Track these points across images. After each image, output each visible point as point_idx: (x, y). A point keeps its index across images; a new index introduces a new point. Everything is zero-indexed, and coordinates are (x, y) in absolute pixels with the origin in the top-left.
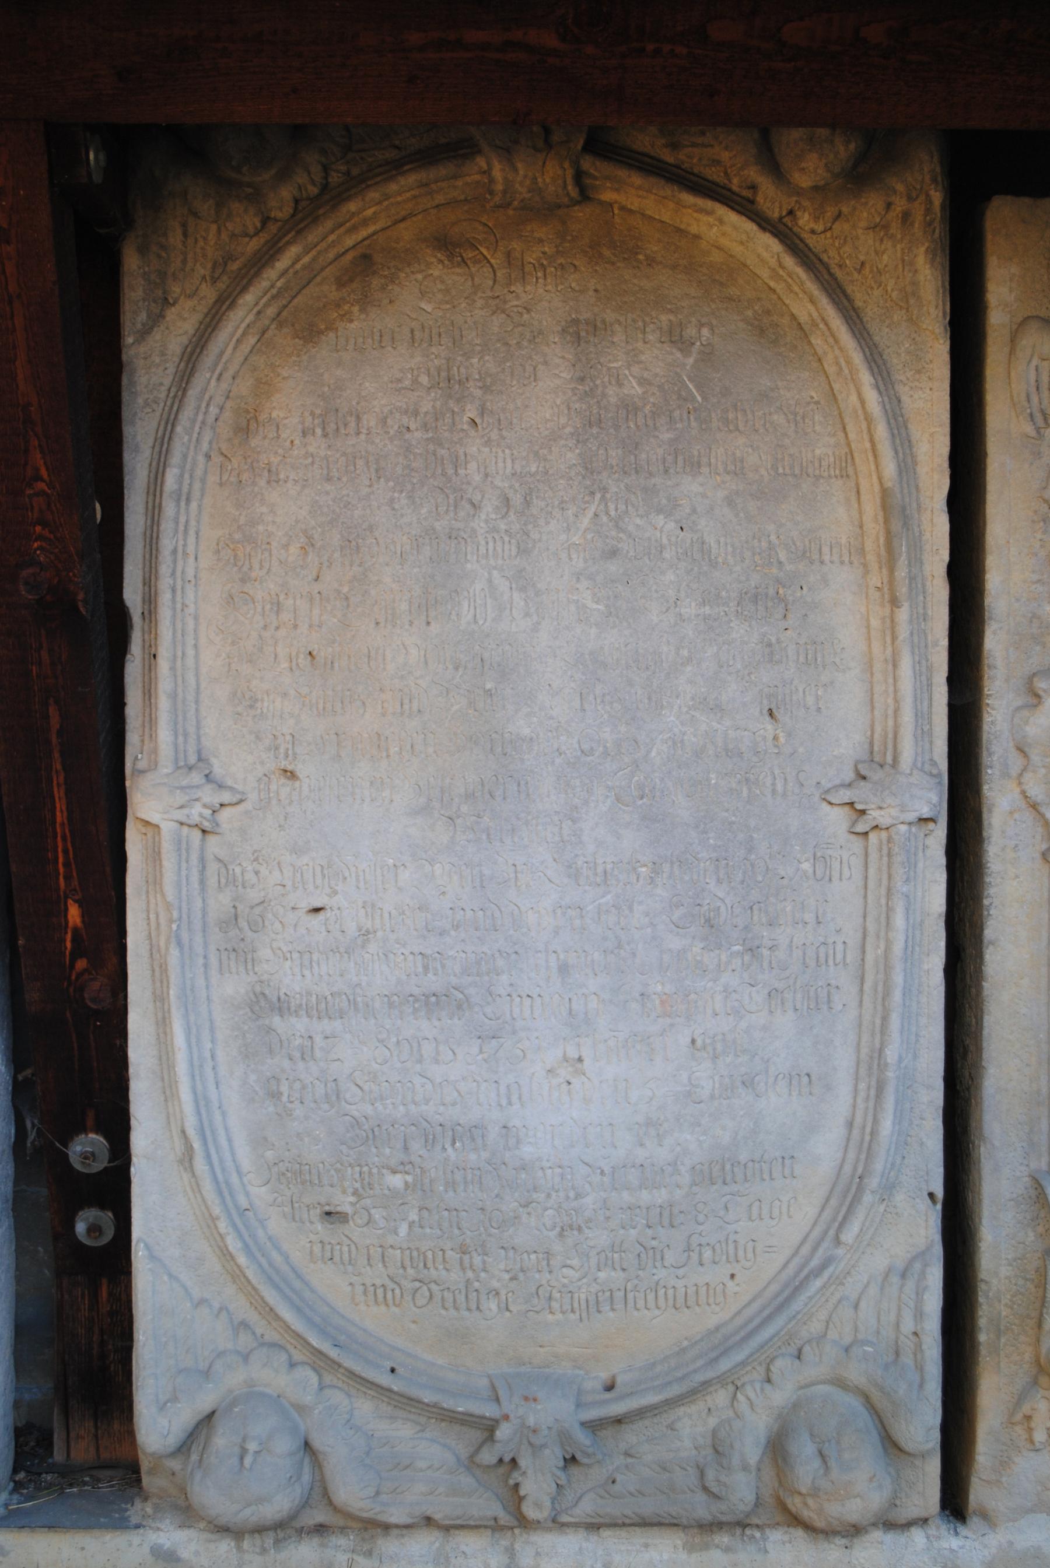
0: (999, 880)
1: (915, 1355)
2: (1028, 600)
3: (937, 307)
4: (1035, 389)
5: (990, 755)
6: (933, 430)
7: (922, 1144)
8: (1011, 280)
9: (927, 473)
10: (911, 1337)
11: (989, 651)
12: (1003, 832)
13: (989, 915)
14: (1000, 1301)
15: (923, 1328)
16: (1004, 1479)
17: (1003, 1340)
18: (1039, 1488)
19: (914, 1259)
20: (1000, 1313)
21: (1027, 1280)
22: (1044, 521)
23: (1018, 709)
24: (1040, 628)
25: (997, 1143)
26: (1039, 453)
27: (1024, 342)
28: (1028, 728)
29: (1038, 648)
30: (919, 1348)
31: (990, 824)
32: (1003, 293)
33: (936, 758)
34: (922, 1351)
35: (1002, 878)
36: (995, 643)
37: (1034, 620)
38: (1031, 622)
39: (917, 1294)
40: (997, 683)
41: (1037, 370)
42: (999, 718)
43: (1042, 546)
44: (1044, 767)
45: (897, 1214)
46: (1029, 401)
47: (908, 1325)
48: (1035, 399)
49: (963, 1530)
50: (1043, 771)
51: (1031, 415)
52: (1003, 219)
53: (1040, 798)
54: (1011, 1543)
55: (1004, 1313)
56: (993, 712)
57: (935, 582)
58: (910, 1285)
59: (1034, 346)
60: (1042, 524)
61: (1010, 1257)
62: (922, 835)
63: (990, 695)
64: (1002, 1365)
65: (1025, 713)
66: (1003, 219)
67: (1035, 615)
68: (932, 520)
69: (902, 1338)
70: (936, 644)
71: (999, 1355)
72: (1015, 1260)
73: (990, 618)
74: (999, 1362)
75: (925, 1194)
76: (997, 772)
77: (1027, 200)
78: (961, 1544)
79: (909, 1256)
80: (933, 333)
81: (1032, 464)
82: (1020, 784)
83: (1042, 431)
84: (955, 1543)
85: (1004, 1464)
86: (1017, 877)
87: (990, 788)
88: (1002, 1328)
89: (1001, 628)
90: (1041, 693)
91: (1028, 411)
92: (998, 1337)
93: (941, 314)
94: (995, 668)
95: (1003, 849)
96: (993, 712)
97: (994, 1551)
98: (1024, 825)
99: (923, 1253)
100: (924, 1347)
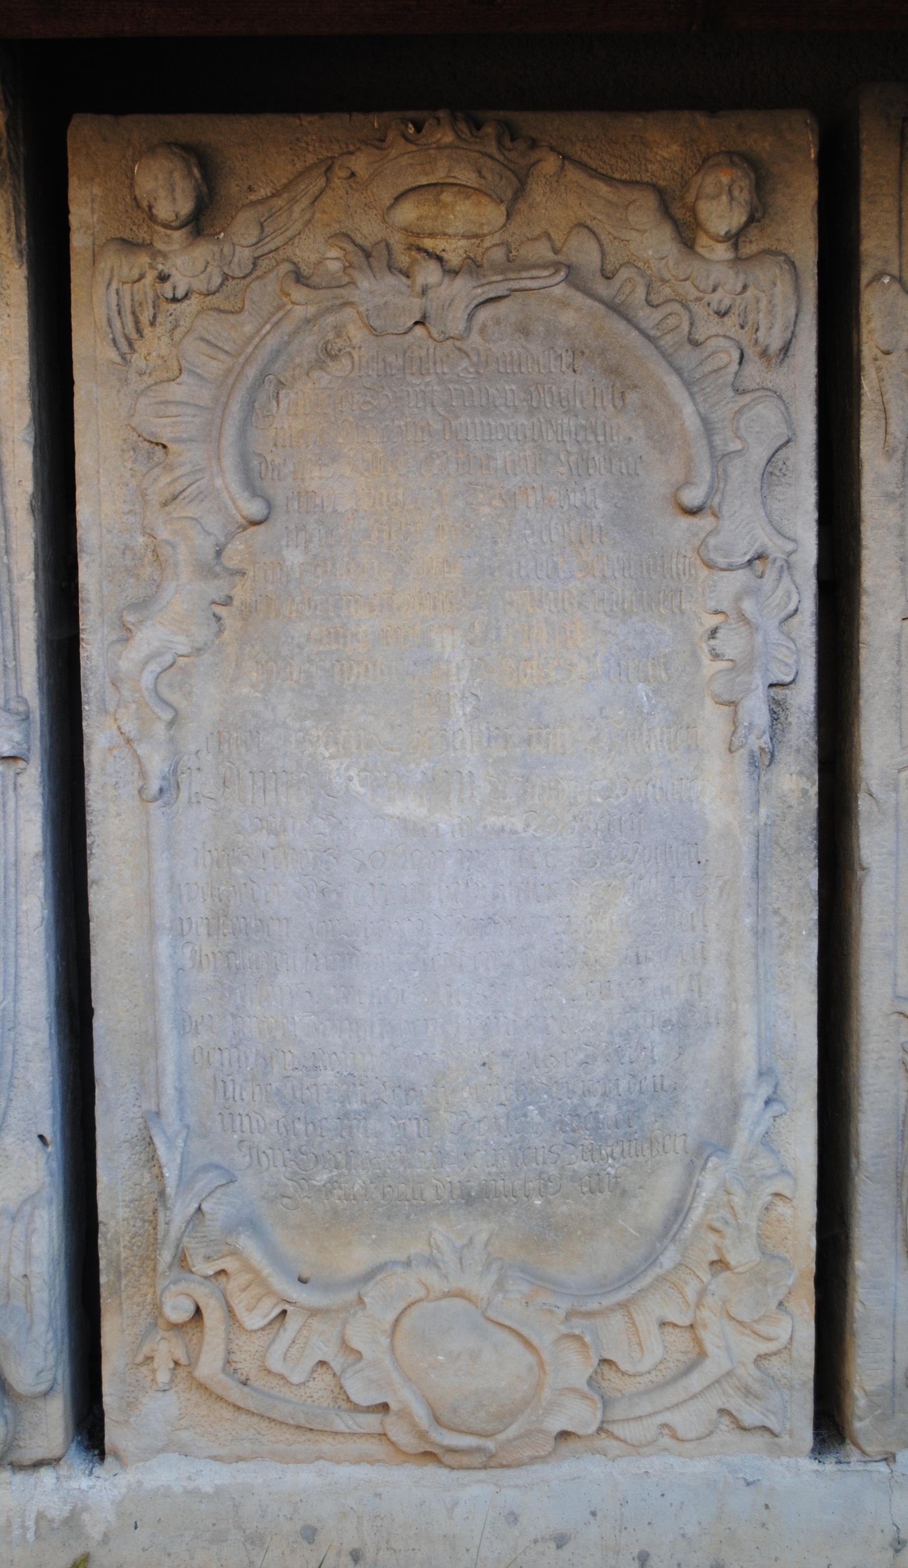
0: (100, 818)
1: (26, 1296)
2: (120, 531)
3: (8, 230)
4: (116, 314)
5: (87, 690)
6: (12, 358)
7: (29, 1086)
8: (93, 201)
9: (7, 402)
10: (20, 1279)
11: (83, 584)
12: (103, 769)
13: (91, 853)
14: (118, 1243)
15: (31, 1271)
16: (132, 1420)
17: (124, 1282)
18: (169, 1428)
19: (24, 1202)
20: (119, 1255)
21: (145, 1221)
22: (134, 450)
23: (113, 643)
24: (133, 559)
25: (108, 1085)
26: (126, 380)
27: (102, 265)
28: (121, 663)
29: (132, 580)
30: (28, 1293)
31: (89, 761)
32: (876, 244)
33: (26, 694)
34: (31, 1294)
35: (104, 816)
36: (89, 576)
37: (128, 552)
38: (124, 553)
39: (27, 1236)
40: (91, 617)
41: (117, 293)
42: (94, 653)
43: (132, 476)
44: (134, 702)
45: (7, 1156)
46: (111, 327)
47: (18, 1268)
48: (117, 324)
49: (98, 1471)
50: (133, 706)
51: (114, 341)
52: (84, 136)
53: (132, 735)
54: (140, 1483)
55: (123, 1255)
56: (88, 647)
57: (18, 514)
58: (20, 1227)
59: (112, 269)
60: (132, 453)
61: (127, 1199)
62: (12, 774)
63: (84, 630)
64: (125, 1307)
65: (119, 647)
66: (84, 136)
67: (127, 547)
68: (13, 450)
69: (12, 1281)
70: (21, 578)
71: (120, 1297)
72: (132, 1201)
73: (82, 551)
74: (121, 1304)
75: (35, 1137)
76: (94, 708)
77: (107, 117)
78: (91, 1483)
79: (22, 1198)
80: (6, 256)
81: (119, 391)
82: (116, 720)
83: (128, 356)
84: (85, 1483)
85: (131, 1405)
86: (119, 815)
87: (88, 725)
88: (123, 1269)
89: (93, 561)
90: (131, 627)
91: (111, 336)
92: (119, 1278)
93: (14, 238)
94: (88, 602)
95: (103, 786)
96: (88, 647)
97: (123, 1490)
98: (124, 762)
99: (33, 1196)
100: (33, 1289)
